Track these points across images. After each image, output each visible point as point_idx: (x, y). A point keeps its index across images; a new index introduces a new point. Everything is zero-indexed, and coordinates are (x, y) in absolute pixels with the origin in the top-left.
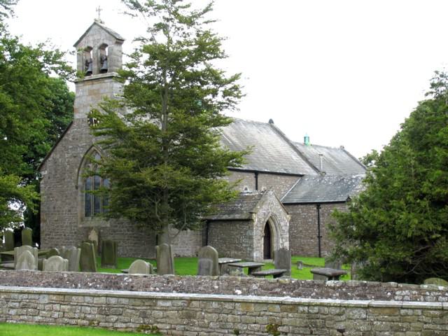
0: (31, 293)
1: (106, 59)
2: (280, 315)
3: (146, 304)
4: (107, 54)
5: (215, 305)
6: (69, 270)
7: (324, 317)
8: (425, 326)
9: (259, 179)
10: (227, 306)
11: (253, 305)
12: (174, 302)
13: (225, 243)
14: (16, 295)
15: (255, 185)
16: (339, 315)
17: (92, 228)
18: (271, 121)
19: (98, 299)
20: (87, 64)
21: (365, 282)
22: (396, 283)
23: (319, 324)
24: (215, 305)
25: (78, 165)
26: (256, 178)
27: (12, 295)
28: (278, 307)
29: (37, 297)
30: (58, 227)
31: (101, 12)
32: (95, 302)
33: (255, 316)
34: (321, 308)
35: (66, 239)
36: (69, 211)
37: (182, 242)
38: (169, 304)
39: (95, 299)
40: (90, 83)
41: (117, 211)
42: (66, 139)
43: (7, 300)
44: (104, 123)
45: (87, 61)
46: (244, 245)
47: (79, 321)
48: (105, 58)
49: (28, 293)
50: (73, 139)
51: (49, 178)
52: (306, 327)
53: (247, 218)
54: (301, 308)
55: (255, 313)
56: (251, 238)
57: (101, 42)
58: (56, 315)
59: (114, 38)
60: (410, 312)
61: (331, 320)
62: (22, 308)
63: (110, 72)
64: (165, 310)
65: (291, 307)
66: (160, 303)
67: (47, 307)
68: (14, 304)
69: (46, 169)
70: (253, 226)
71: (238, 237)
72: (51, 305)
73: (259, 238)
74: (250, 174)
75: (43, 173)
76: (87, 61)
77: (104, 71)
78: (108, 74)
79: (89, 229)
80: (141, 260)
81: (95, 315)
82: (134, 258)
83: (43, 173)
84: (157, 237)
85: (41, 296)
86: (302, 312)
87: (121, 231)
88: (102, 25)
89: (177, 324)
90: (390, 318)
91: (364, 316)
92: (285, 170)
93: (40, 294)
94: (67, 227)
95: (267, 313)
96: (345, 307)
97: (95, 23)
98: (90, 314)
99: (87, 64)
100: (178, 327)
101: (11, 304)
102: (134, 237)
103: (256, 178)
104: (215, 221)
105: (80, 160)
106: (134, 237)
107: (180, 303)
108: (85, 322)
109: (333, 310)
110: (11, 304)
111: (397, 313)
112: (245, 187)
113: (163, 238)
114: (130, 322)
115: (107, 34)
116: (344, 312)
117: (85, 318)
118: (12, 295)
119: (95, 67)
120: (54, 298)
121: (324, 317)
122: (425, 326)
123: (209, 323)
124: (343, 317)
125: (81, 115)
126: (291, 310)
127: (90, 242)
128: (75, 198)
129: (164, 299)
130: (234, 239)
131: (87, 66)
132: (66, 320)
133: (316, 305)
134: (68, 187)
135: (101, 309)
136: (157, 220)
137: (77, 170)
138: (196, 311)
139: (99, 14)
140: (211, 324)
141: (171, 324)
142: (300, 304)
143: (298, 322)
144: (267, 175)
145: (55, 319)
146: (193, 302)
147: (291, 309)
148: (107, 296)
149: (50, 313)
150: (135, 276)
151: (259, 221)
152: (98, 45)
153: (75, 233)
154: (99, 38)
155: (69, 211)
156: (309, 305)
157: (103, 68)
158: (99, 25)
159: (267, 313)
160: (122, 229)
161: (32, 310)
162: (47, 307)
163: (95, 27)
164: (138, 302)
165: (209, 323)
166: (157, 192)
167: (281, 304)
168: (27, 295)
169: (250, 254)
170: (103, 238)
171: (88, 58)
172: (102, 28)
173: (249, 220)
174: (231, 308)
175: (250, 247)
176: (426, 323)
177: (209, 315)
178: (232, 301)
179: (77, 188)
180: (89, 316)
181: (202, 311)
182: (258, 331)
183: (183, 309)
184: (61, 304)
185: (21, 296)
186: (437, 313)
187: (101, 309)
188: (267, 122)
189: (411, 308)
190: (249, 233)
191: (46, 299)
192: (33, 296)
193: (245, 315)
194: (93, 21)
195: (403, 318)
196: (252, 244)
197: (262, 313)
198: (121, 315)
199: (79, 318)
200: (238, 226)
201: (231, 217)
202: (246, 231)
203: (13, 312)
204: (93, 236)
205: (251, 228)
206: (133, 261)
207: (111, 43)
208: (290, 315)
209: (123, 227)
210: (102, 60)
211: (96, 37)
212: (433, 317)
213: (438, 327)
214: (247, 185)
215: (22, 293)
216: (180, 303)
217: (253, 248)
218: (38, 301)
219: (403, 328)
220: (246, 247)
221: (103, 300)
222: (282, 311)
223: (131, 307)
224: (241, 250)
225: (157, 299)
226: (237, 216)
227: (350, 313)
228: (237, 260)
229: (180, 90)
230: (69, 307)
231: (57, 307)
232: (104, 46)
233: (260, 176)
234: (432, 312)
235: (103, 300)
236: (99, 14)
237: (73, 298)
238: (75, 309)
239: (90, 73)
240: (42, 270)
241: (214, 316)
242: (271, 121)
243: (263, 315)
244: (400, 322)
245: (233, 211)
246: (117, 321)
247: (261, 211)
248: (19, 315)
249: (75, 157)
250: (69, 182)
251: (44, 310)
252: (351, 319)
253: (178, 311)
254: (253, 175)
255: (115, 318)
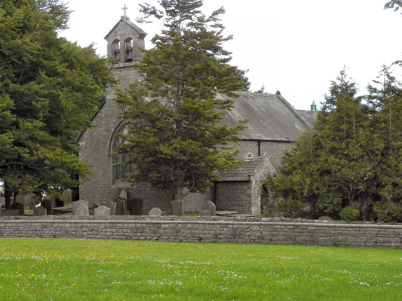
0: (95, 223)
1: (131, 50)
2: (220, 229)
3: (156, 226)
4: (132, 46)
5: (189, 225)
6: (111, 215)
7: (240, 230)
8: (287, 233)
9: (261, 146)
10: (196, 226)
11: (207, 225)
12: (169, 224)
13: (229, 200)
14: (87, 224)
15: (257, 152)
16: (246, 228)
17: (122, 189)
18: (278, 93)
19: (131, 224)
20: (116, 53)
21: (284, 218)
22: (301, 218)
23: (238, 233)
24: (189, 225)
25: (110, 137)
26: (259, 145)
27: (84, 225)
28: (219, 225)
29: (98, 225)
30: (94, 188)
31: (126, 10)
32: (129, 226)
33: (209, 230)
34: (239, 225)
35: (101, 198)
36: (104, 175)
37: (190, 199)
38: (167, 226)
39: (129, 225)
40: (119, 70)
41: (143, 176)
42: (99, 116)
43: (82, 227)
44: (131, 105)
45: (115, 51)
46: (244, 202)
47: (121, 236)
48: (130, 49)
49: (93, 223)
50: (106, 116)
51: (86, 148)
52: (232, 235)
53: (246, 179)
54: (229, 226)
55: (208, 229)
56: (249, 196)
57: (127, 36)
58: (108, 234)
59: (137, 34)
60: (279, 227)
61: (244, 231)
62: (90, 231)
63: (135, 61)
64: (165, 229)
65: (225, 225)
66: (163, 225)
67: (104, 230)
68: (86, 229)
69: (83, 141)
70: (251, 186)
71: (239, 195)
72: (106, 229)
73: (257, 196)
74: (253, 143)
75: (80, 144)
76: (115, 51)
77: (130, 60)
78: (133, 63)
79: (120, 190)
80: (157, 208)
81: (129, 233)
82: (154, 206)
83: (80, 144)
84: (174, 195)
85: (101, 224)
86: (230, 228)
87: (145, 191)
88: (127, 21)
89: (171, 236)
90: (270, 230)
91: (258, 229)
92: (286, 138)
93: (100, 223)
94: (101, 188)
95: (214, 229)
96: (249, 225)
97: (121, 20)
98: (127, 233)
99: (116, 53)
100: (171, 238)
101: (83, 229)
102: (156, 196)
103: (259, 145)
104: (222, 182)
105: (111, 133)
106: (156, 196)
107: (172, 225)
108: (124, 237)
109: (244, 226)
110: (83, 229)
111: (273, 227)
112: (249, 153)
113: (178, 196)
114: (148, 236)
115: (132, 30)
116: (249, 227)
117: (124, 235)
118: (84, 225)
119: (122, 56)
120: (108, 225)
121: (240, 230)
122: (287, 233)
123: (187, 235)
124: (249, 230)
125: (111, 96)
126: (225, 227)
127: (121, 198)
128: (108, 165)
129: (165, 223)
130: (236, 197)
131: (115, 55)
132: (114, 236)
133: (236, 224)
134: (102, 155)
135: (133, 230)
136: (172, 182)
137: (109, 142)
138: (180, 229)
139: (125, 12)
140: (188, 235)
141: (168, 236)
142: (229, 224)
143: (228, 233)
144: (269, 143)
145: (108, 236)
146: (179, 225)
147: (225, 226)
148: (135, 223)
149: (105, 233)
150: (152, 217)
151: (256, 182)
152: (125, 38)
153: (108, 193)
154: (125, 33)
155: (104, 175)
156: (233, 224)
157: (129, 58)
158: (125, 22)
159: (214, 229)
160: (147, 189)
161: (96, 232)
162: (104, 230)
163: (122, 23)
164: (152, 225)
165: (187, 235)
166: (173, 161)
167: (220, 224)
168: (92, 224)
169: (249, 209)
170: (131, 197)
171: (116, 49)
172: (127, 24)
173: (248, 182)
174: (197, 227)
175: (249, 203)
176: (287, 232)
177: (187, 231)
178: (198, 223)
179: (109, 156)
180: (126, 234)
181: (183, 229)
182: (210, 238)
183: (174, 228)
184: (111, 228)
185: (89, 225)
186: (292, 227)
187: (133, 230)
188: (274, 93)
189: (280, 225)
190: (248, 191)
191: (102, 226)
192: (96, 225)
193: (204, 230)
194: (120, 19)
195: (276, 230)
196: (251, 201)
197: (212, 229)
198: (143, 232)
199: (121, 235)
200: (239, 186)
201: (234, 179)
202: (245, 190)
203: (85, 233)
204: (123, 195)
205: (249, 188)
206: (153, 208)
207: (135, 37)
208: (225, 229)
209: (147, 188)
210: (128, 51)
211: (124, 32)
212: (290, 229)
213: (292, 234)
214: (250, 152)
215: (90, 223)
216: (172, 225)
217: (251, 204)
218: (98, 227)
219: (276, 234)
220: (246, 203)
221: (133, 225)
222: (221, 227)
223: (148, 228)
224: (242, 206)
225: (161, 224)
226: (239, 179)
227: (252, 228)
228: (234, 212)
229: (193, 65)
230: (115, 229)
231: (109, 230)
232: (128, 40)
233: (262, 144)
234: (289, 227)
235: (133, 225)
236: (125, 12)
237: (118, 224)
238: (119, 231)
239: (117, 62)
240: (93, 215)
241: (189, 231)
242: (278, 93)
243: (212, 230)
244: (274, 231)
245: (236, 174)
246: (141, 236)
247: (258, 174)
248: (89, 235)
249: (107, 131)
250: (103, 151)
251: (102, 232)
252: (252, 230)
253: (171, 229)
254: (256, 144)
255: (140, 234)
